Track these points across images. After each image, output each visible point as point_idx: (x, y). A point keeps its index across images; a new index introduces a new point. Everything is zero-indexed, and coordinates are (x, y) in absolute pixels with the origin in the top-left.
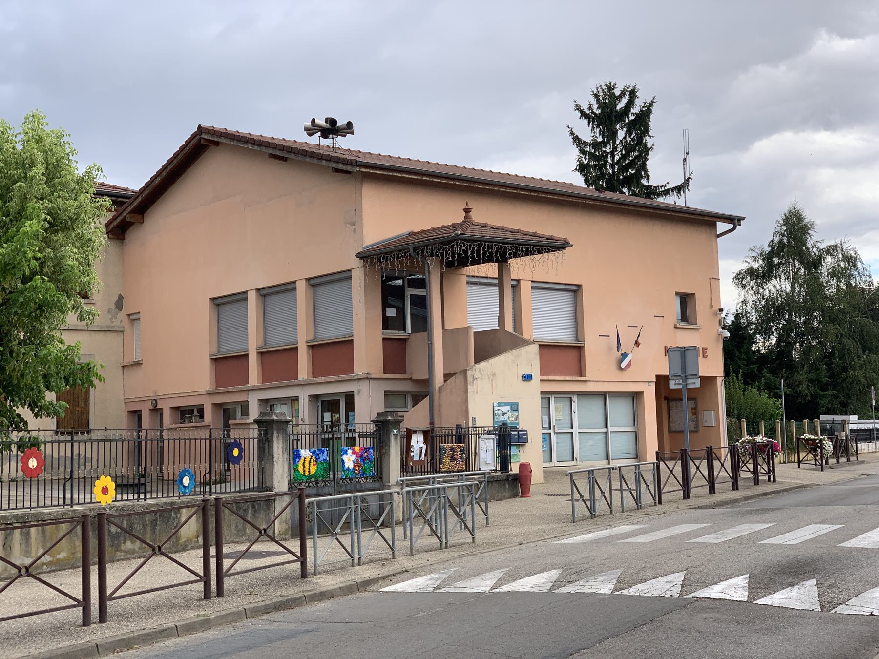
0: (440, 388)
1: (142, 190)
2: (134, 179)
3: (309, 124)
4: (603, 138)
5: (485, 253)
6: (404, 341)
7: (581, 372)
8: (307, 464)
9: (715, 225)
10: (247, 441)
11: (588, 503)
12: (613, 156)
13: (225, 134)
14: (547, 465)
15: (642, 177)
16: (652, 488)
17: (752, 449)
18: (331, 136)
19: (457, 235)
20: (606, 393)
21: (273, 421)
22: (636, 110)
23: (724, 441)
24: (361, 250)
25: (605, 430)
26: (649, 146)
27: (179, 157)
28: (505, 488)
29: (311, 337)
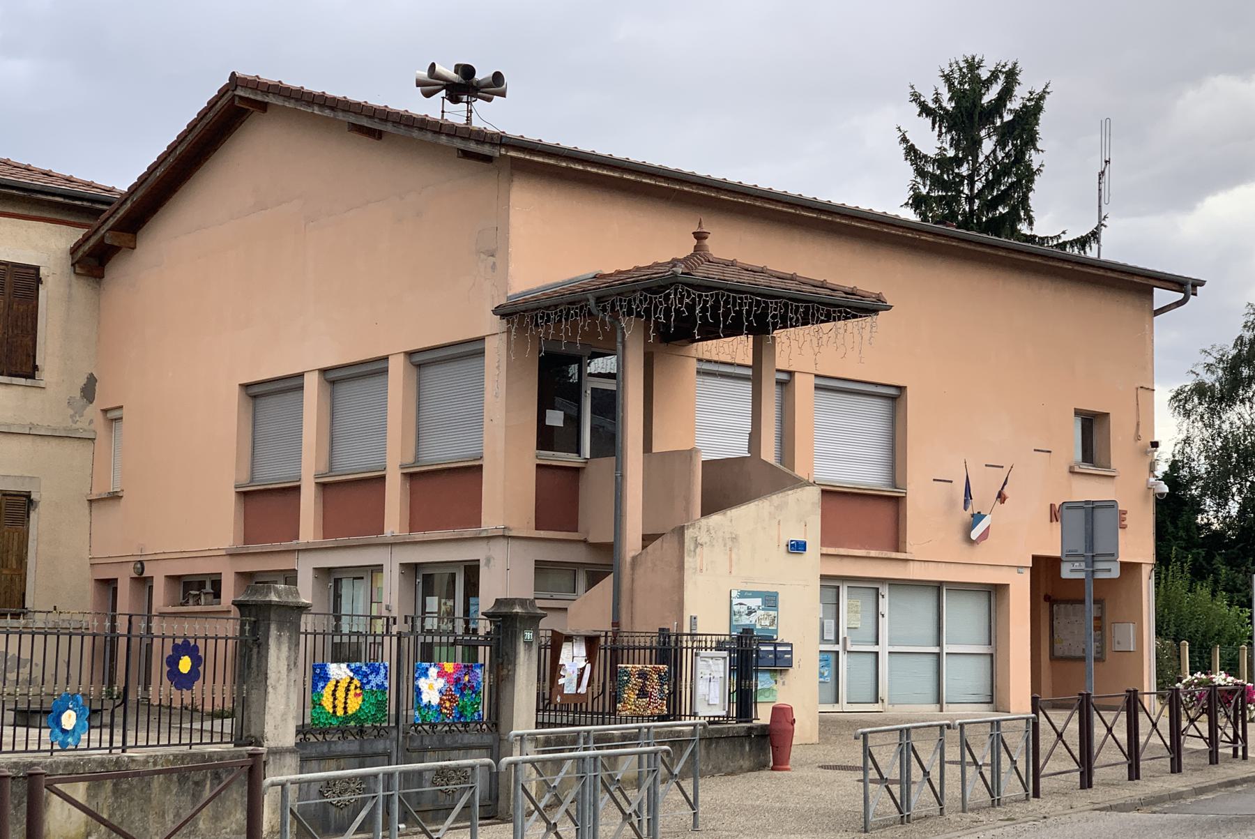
0: (634, 559)
1: (134, 189)
2: (118, 170)
3: (424, 74)
4: (957, 149)
5: (726, 315)
6: (577, 470)
7: (897, 543)
8: (340, 694)
9: (1151, 293)
10: (211, 643)
11: (896, 789)
12: (972, 184)
13: (279, 90)
14: (829, 708)
15: (1020, 220)
16: (1022, 767)
17: (1209, 699)
18: (465, 98)
19: (674, 274)
20: (941, 583)
21: (269, 605)
22: (1015, 104)
23: (1149, 682)
24: (504, 301)
25: (936, 650)
26: (1035, 167)
27: (196, 131)
28: (742, 755)
29: (410, 459)
